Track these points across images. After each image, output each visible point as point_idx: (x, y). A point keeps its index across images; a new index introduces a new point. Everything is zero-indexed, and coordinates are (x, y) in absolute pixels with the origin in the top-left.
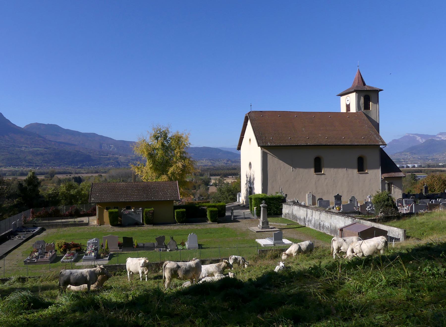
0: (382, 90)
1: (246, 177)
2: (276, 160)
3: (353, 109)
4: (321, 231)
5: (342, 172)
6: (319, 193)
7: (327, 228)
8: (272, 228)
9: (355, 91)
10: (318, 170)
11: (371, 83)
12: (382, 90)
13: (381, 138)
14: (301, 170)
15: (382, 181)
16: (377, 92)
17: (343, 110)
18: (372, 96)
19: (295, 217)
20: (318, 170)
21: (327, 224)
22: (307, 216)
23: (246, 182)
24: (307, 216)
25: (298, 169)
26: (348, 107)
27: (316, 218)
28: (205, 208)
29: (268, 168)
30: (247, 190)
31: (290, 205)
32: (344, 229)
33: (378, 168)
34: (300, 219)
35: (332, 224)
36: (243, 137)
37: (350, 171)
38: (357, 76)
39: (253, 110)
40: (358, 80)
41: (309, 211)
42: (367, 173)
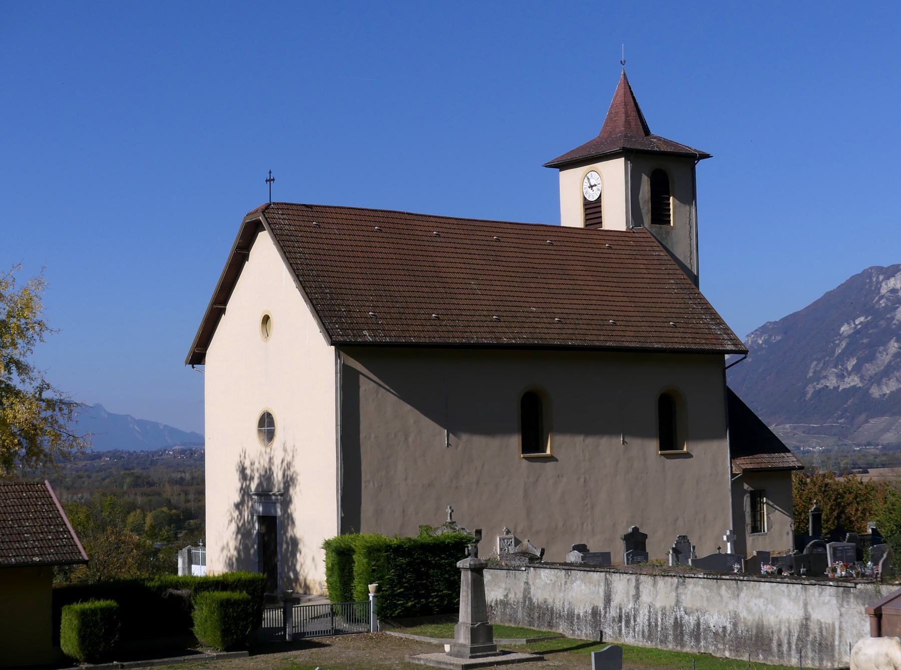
0: (708, 156)
1: (236, 477)
2: (390, 399)
3: (615, 218)
4: (687, 649)
5: (610, 449)
6: (538, 532)
7: (720, 636)
8: (504, 653)
9: (626, 153)
10: (533, 444)
11: (668, 128)
12: (708, 156)
13: (727, 329)
14: (479, 441)
15: (733, 483)
16: (689, 159)
17: (572, 216)
18: (675, 173)
19: (546, 613)
20: (533, 444)
21: (715, 619)
22: (608, 600)
23: (237, 498)
24: (608, 600)
25: (465, 437)
26: (593, 209)
27: (658, 605)
28: (184, 592)
29: (362, 435)
30: (243, 532)
31: (517, 569)
32: (885, 611)
33: (722, 437)
34: (571, 617)
35: (743, 614)
36: (222, 311)
37: (636, 444)
38: (620, 98)
39: (281, 196)
40: (627, 116)
41: (622, 585)
42: (688, 455)
